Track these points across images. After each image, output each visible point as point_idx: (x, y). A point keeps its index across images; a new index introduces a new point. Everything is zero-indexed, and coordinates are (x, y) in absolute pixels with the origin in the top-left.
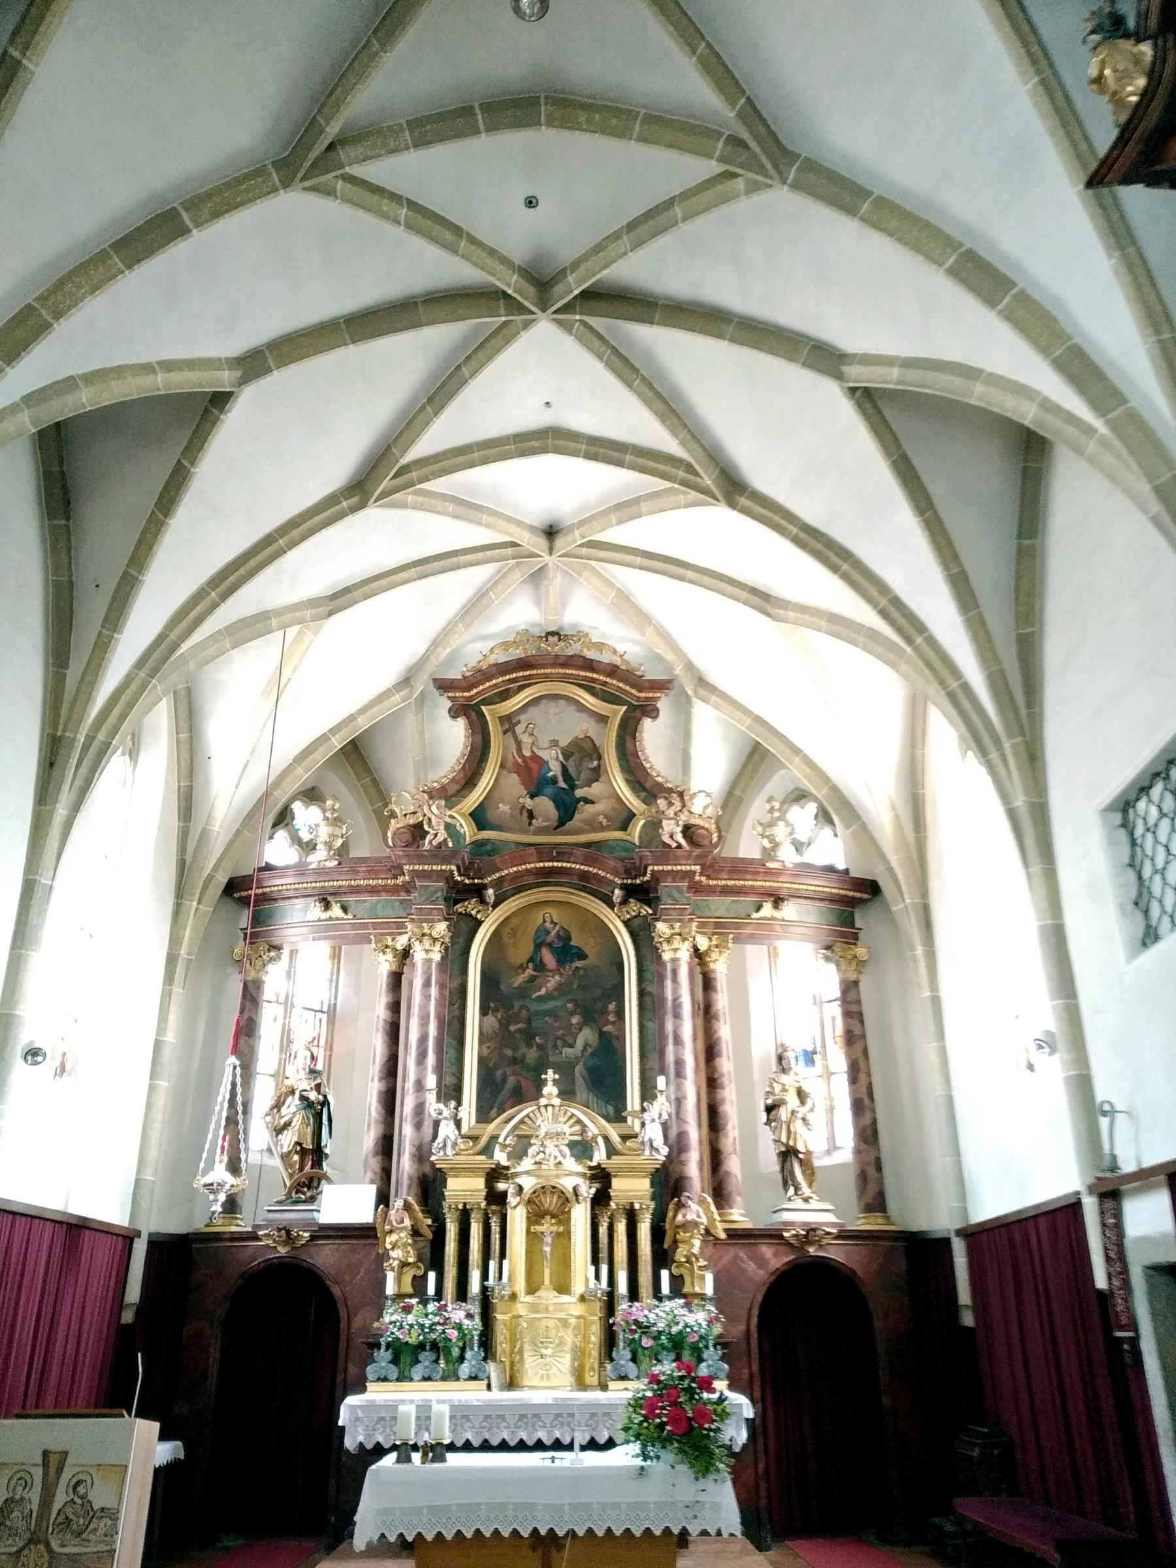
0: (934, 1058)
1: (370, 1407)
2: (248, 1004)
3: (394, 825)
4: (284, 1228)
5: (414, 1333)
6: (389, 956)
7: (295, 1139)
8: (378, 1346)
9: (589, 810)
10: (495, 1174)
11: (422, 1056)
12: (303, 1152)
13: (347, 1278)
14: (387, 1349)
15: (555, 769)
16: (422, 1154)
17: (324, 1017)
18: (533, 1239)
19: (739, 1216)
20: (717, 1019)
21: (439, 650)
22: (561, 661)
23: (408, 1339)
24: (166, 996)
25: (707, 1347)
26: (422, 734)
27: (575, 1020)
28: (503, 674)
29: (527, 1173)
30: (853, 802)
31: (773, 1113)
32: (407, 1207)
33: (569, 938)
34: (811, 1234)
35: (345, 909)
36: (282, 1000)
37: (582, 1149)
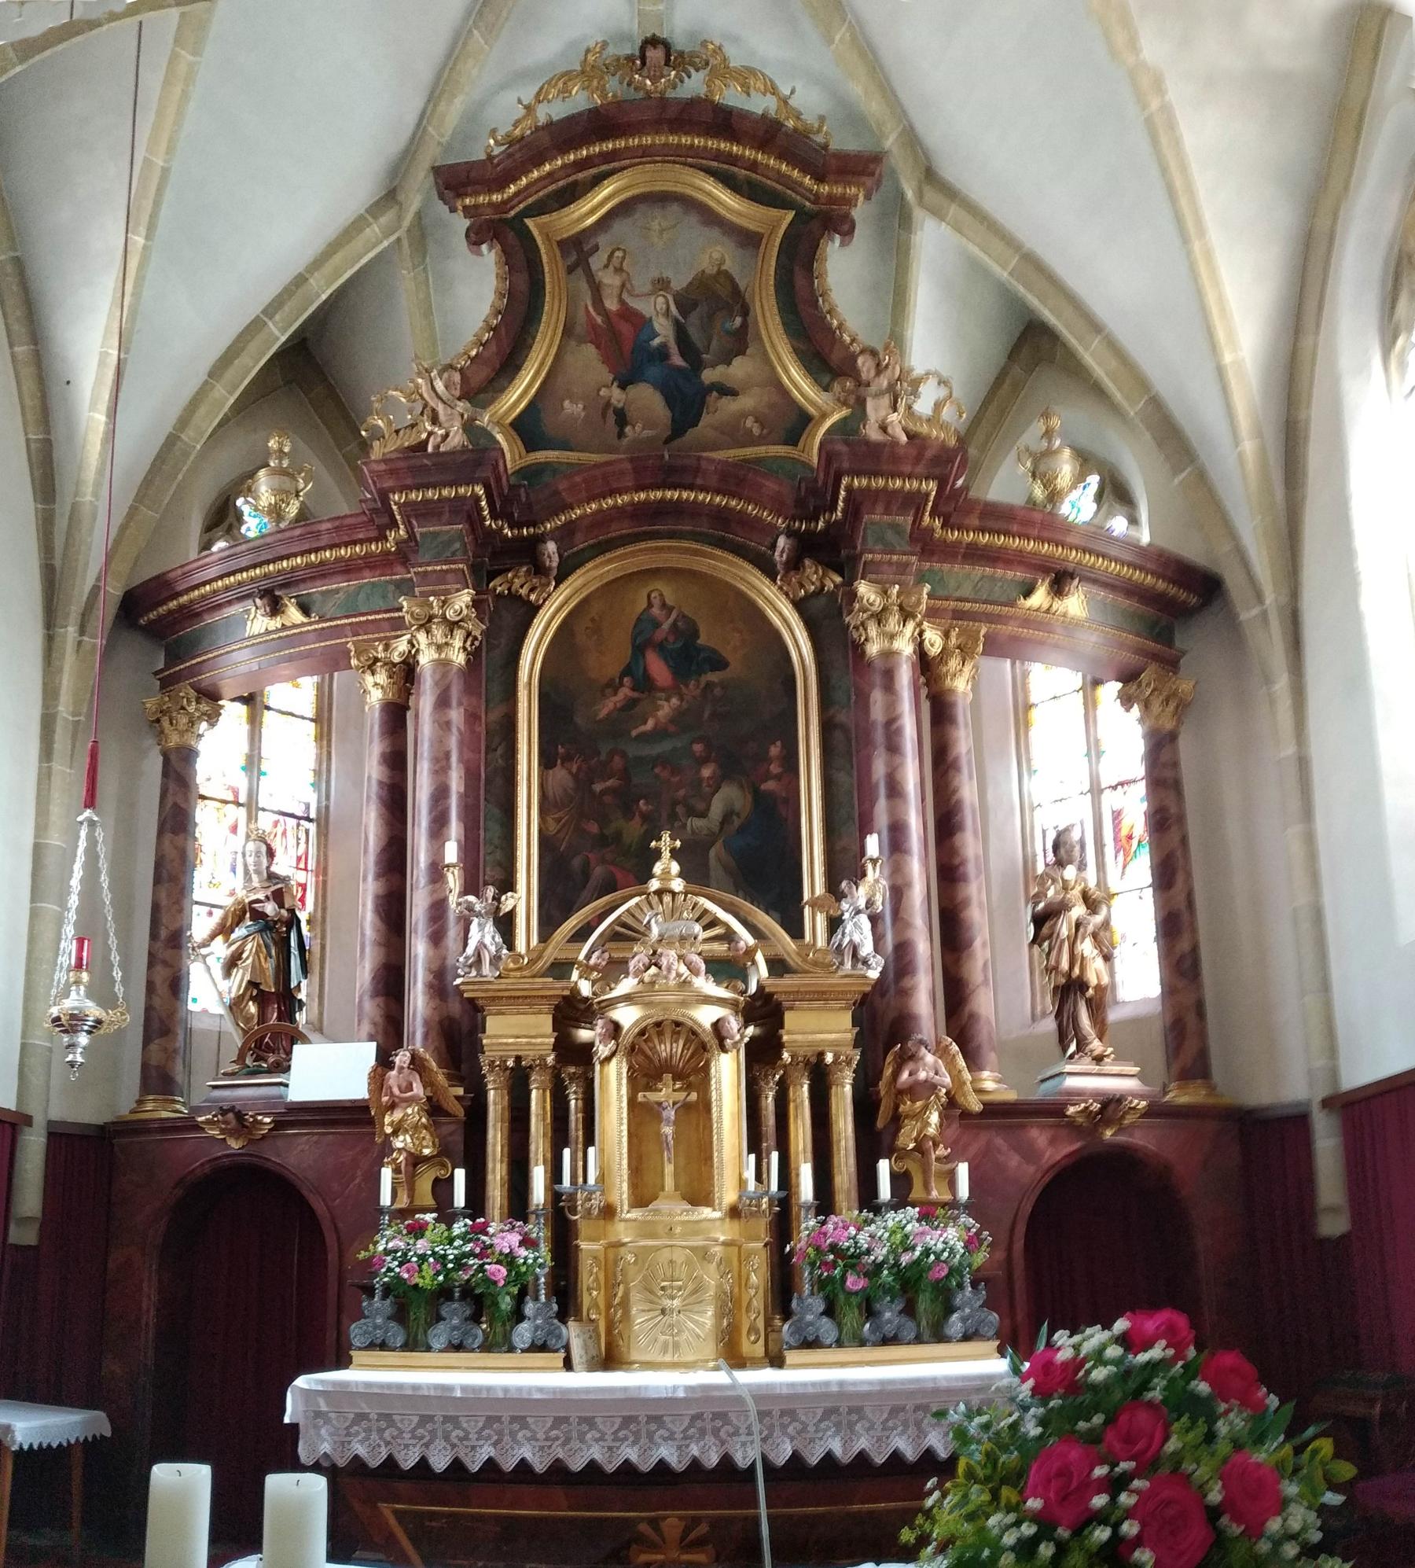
0: (1297, 848)
1: (340, 1394)
2: (172, 786)
3: (377, 451)
4: (232, 1109)
5: (428, 1270)
6: (382, 677)
7: (247, 977)
8: (370, 1291)
9: (729, 407)
10: (571, 1012)
11: (439, 823)
12: (262, 999)
13: (335, 1186)
14: (384, 1297)
15: (663, 331)
16: (440, 984)
17: (312, 828)
18: (641, 1115)
19: (991, 1084)
20: (958, 769)
21: (442, 107)
22: (671, 113)
23: (416, 1280)
24: (45, 778)
25: (960, 1286)
26: (428, 313)
27: (706, 772)
28: (564, 147)
29: (628, 999)
30: (1189, 430)
31: (1047, 925)
32: (416, 1063)
33: (695, 634)
34: (1111, 1104)
35: (305, 610)
36: (242, 799)
37: (726, 968)
